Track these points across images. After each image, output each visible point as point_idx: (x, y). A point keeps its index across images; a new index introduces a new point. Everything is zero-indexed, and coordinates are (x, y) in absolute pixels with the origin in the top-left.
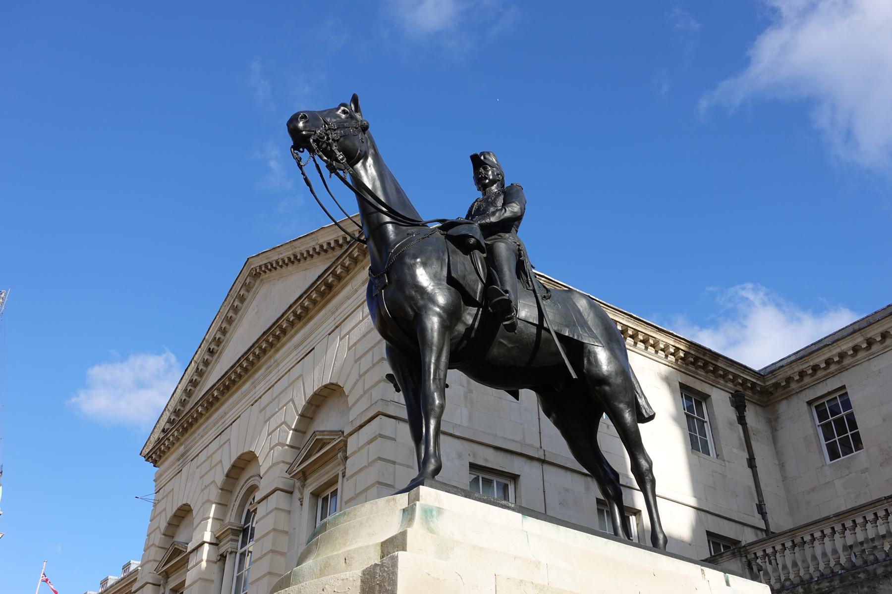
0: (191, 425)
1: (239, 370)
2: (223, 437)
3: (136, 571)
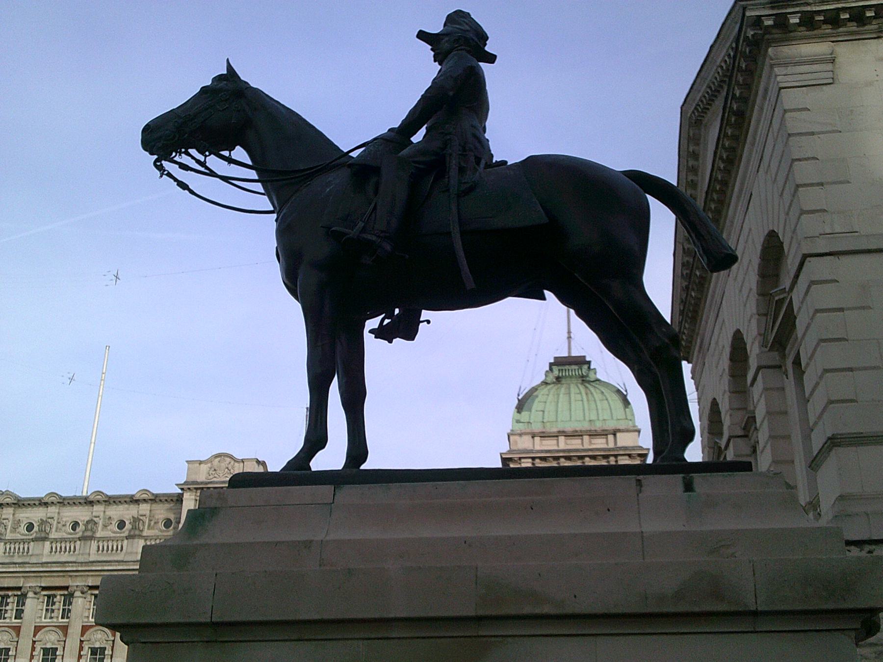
0: (695, 312)
1: (715, 196)
2: (720, 319)
3: (727, 156)
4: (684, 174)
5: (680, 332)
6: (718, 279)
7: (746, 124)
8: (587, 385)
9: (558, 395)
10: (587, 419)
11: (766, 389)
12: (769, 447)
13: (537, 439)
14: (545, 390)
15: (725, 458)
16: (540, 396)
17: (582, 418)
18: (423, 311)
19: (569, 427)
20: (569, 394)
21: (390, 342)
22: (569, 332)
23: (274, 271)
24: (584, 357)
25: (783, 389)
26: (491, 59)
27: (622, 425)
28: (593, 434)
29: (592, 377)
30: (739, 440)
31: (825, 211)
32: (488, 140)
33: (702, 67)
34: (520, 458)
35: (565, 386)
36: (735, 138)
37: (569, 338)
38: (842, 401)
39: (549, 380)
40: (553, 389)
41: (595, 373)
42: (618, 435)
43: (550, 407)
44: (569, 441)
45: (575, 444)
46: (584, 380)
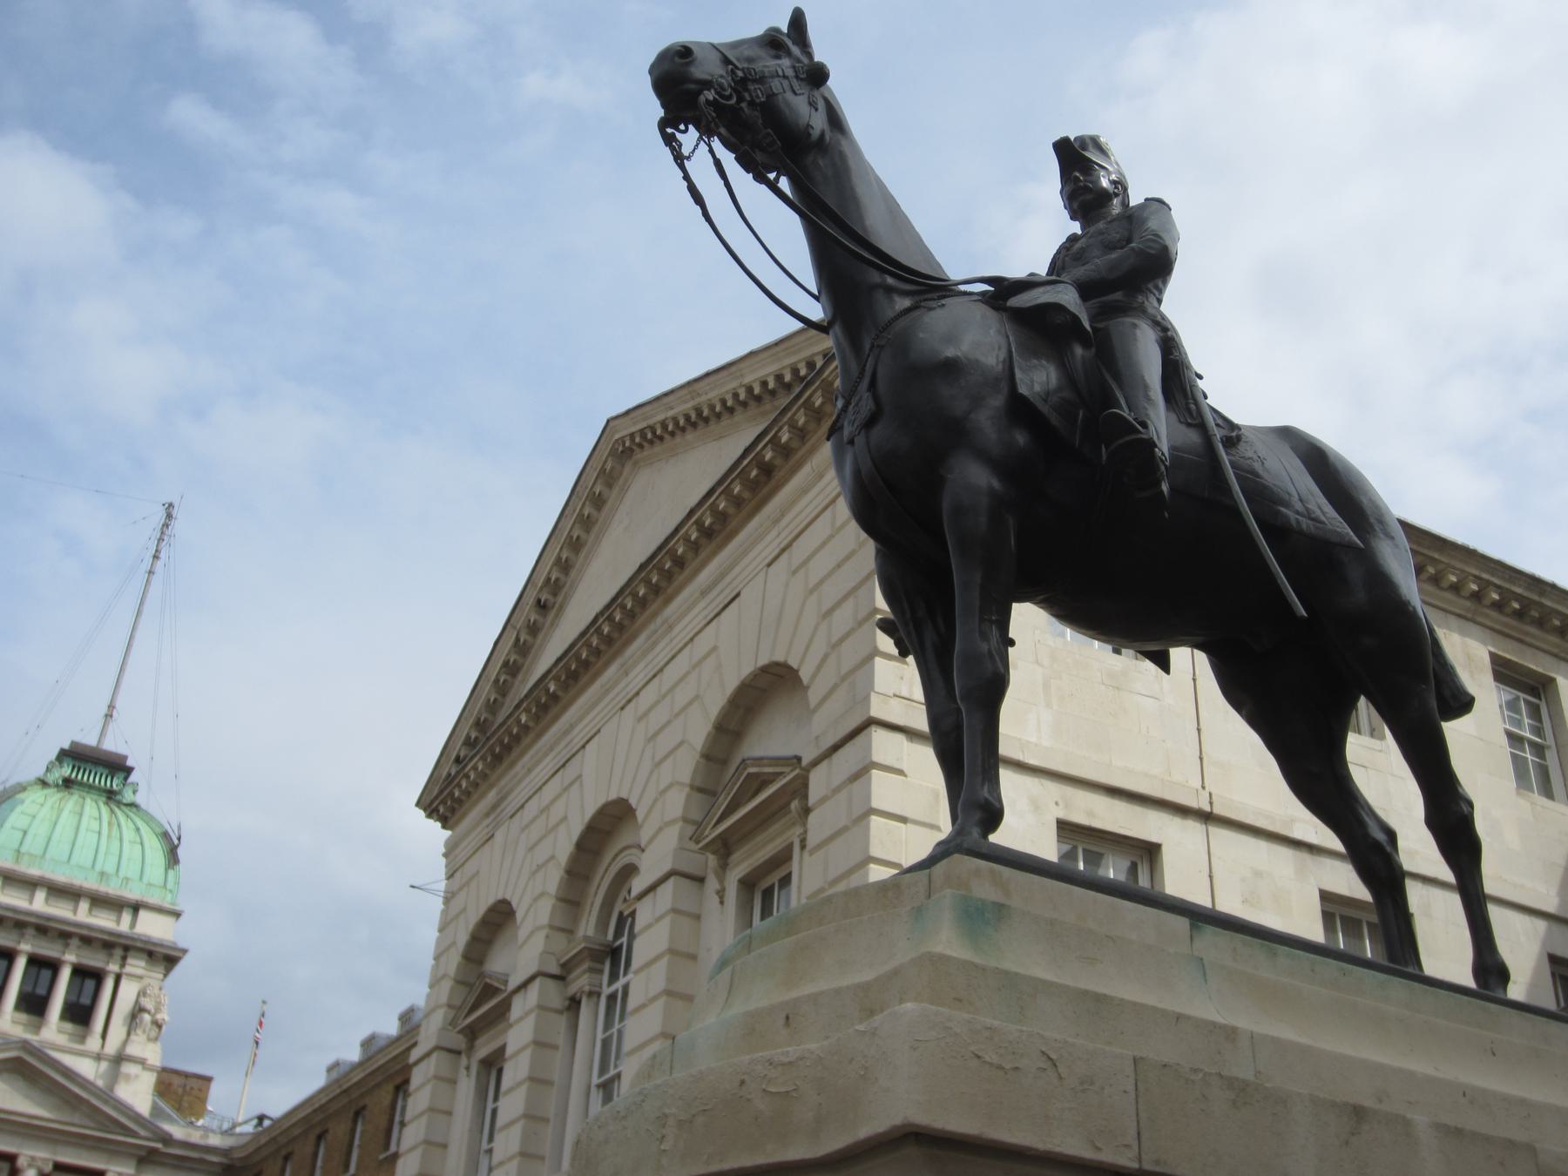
0: (508, 749)
4: (568, 524)
6: (133, 1163)
7: (765, 490)
9: (60, 811)
10: (98, 868)
11: (541, 1007)
12: (428, 1088)
14: (35, 796)
15: (1125, 204)
16: (28, 802)
17: (89, 863)
18: (1015, 605)
19: (61, 876)
20: (81, 815)
21: (418, 804)
22: (111, 707)
23: (652, 58)
24: (126, 758)
25: (698, 917)
27: (154, 898)
29: (128, 796)
30: (549, 982)
31: (900, 772)
32: (1031, 274)
33: (708, 375)
34: (493, 1064)
36: (738, 502)
37: (109, 716)
38: (836, 748)
39: (50, 778)
40: (53, 796)
41: (135, 792)
42: (142, 914)
44: (52, 901)
45: (61, 910)
46: (111, 795)
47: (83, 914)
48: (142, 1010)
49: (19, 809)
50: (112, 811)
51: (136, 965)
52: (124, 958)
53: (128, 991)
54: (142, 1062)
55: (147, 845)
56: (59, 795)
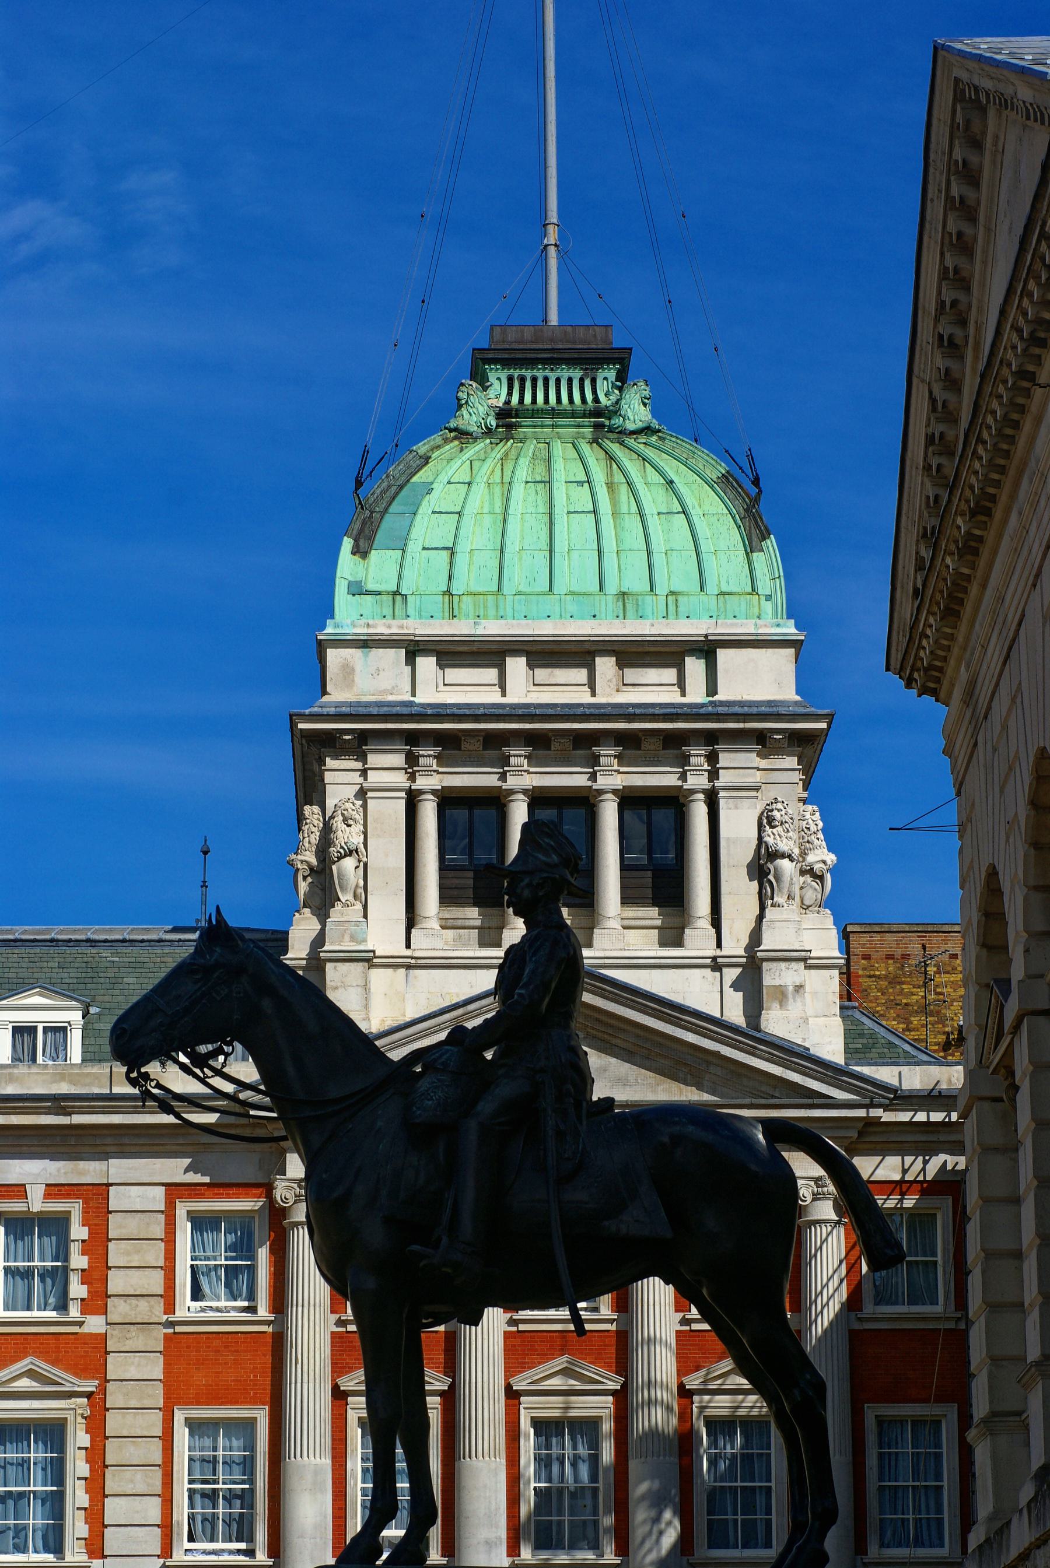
5: (300, 1201)
8: (615, 448)
10: (611, 588)
13: (426, 664)
20: (549, 482)
26: (919, 696)
28: (633, 654)
35: (531, 446)
43: (478, 537)
44: (542, 674)
45: (564, 688)
47: (613, 687)
48: (774, 855)
49: (427, 505)
50: (611, 458)
51: (739, 765)
52: (712, 758)
53: (739, 824)
54: (803, 959)
55: (695, 513)
56: (500, 450)
